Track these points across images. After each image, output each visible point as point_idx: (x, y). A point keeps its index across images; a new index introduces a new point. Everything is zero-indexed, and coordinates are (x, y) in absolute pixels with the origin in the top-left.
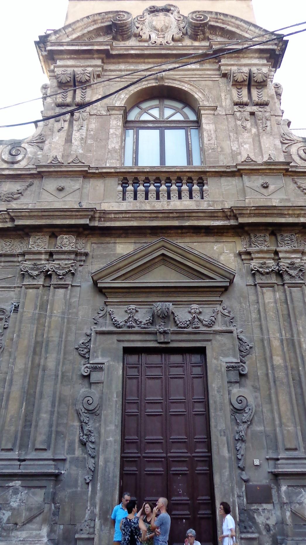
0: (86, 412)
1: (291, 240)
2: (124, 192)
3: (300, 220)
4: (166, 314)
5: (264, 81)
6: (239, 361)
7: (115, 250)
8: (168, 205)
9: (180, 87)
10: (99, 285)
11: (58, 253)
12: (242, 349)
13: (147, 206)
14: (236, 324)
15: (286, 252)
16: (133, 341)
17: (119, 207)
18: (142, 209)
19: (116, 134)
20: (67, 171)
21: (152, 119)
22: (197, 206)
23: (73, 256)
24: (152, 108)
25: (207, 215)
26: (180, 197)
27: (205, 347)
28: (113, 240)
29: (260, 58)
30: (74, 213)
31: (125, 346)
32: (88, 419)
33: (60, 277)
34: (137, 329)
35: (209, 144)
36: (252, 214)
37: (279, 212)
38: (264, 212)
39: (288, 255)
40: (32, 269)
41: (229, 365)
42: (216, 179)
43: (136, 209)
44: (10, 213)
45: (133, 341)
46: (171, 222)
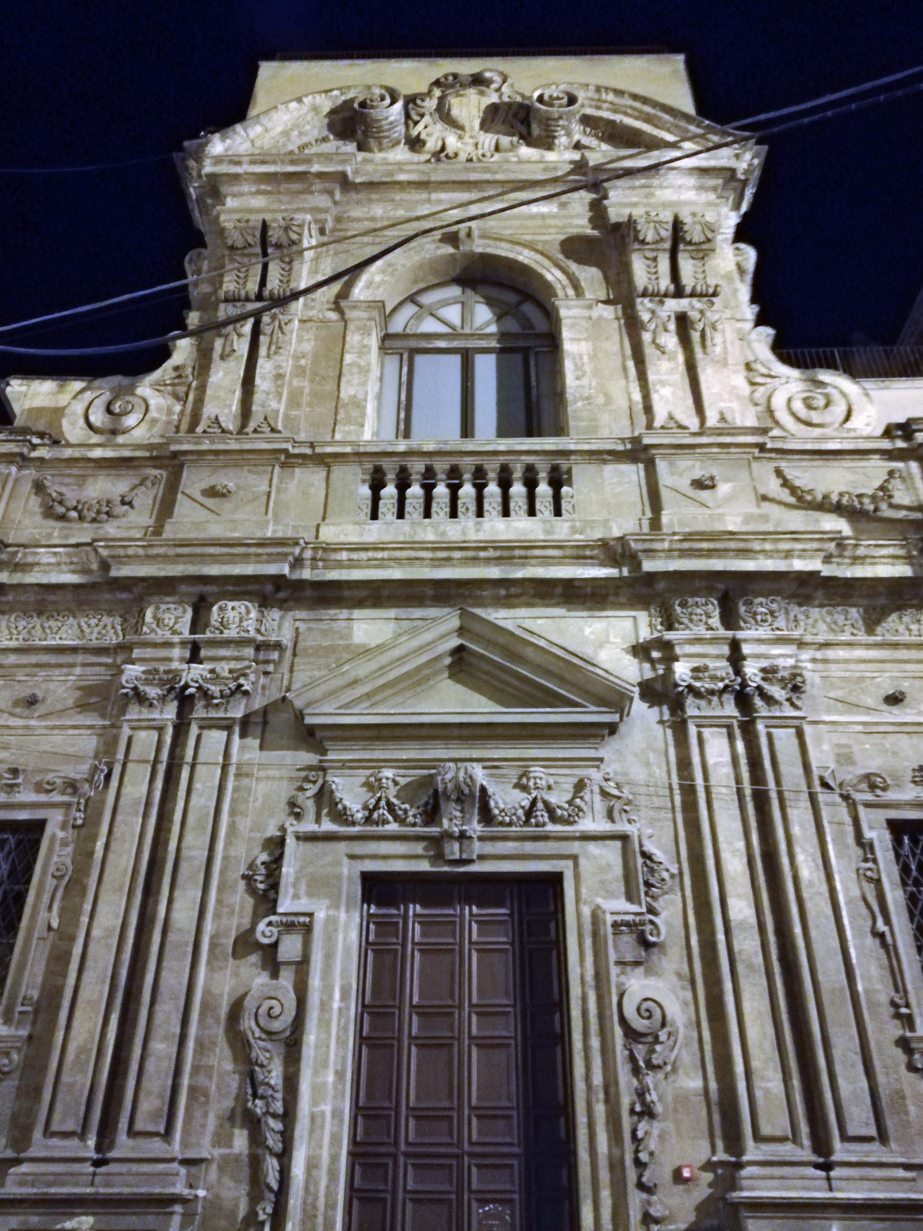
0: (264, 1036)
1: (772, 613)
2: (376, 499)
3: (792, 565)
4: (466, 791)
5: (709, 240)
6: (644, 910)
7: (349, 635)
8: (478, 531)
9: (511, 255)
10: (309, 720)
11: (213, 643)
12: (652, 881)
13: (428, 532)
14: (639, 816)
15: (759, 641)
16: (385, 857)
17: (361, 535)
18: (417, 538)
19: (359, 366)
20: (242, 452)
21: (444, 329)
22: (547, 532)
23: (249, 652)
24: (445, 303)
25: (568, 552)
26: (506, 513)
27: (556, 879)
28: (344, 613)
29: (701, 188)
30: (252, 550)
31: (365, 869)
32: (268, 1055)
33: (215, 701)
34: (393, 827)
35: (577, 387)
36: (675, 550)
37: (741, 545)
38: (704, 545)
39: (763, 649)
40: (148, 682)
41: (618, 918)
42: (593, 468)
43: (401, 539)
44: (100, 550)
45: (385, 857)
46: (481, 569)
